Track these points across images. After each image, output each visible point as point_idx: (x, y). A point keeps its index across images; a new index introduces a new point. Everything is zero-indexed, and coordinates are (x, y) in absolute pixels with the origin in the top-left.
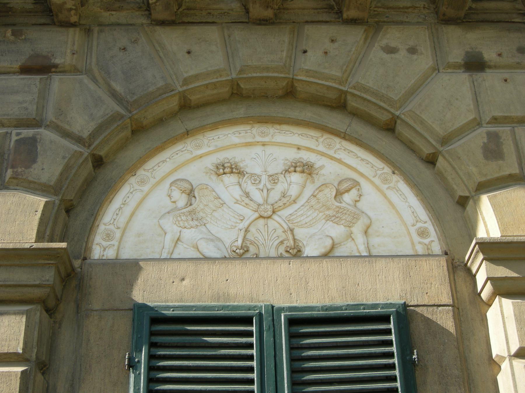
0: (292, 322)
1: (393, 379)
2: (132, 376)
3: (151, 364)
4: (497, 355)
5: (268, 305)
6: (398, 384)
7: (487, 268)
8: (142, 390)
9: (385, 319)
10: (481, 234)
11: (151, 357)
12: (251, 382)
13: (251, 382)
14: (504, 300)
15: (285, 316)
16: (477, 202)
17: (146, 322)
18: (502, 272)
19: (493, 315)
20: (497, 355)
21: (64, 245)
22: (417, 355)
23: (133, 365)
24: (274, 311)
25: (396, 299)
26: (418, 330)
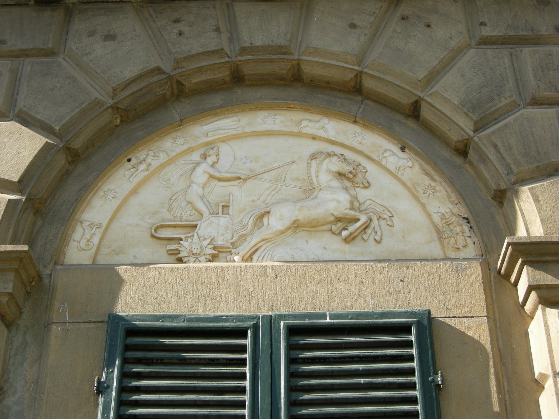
0: (292, 331)
1: (413, 400)
2: (101, 400)
3: (124, 384)
4: (540, 374)
5: (266, 316)
6: (418, 407)
7: (527, 272)
8: (111, 415)
9: (405, 329)
10: (521, 233)
11: (124, 375)
12: (242, 405)
13: (242, 405)
14: (548, 310)
15: (284, 324)
16: (516, 193)
17: (121, 334)
18: (547, 279)
19: (535, 330)
20: (540, 374)
21: (25, 248)
22: (442, 376)
23: (102, 389)
24: (271, 321)
25: (417, 305)
26: (446, 355)
